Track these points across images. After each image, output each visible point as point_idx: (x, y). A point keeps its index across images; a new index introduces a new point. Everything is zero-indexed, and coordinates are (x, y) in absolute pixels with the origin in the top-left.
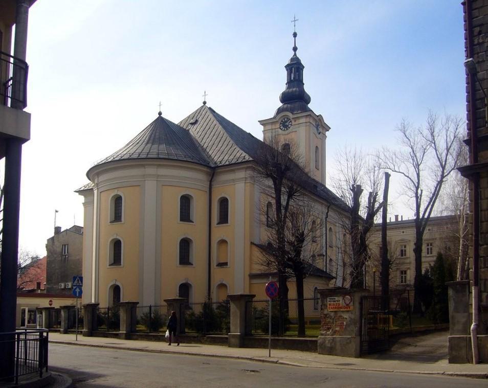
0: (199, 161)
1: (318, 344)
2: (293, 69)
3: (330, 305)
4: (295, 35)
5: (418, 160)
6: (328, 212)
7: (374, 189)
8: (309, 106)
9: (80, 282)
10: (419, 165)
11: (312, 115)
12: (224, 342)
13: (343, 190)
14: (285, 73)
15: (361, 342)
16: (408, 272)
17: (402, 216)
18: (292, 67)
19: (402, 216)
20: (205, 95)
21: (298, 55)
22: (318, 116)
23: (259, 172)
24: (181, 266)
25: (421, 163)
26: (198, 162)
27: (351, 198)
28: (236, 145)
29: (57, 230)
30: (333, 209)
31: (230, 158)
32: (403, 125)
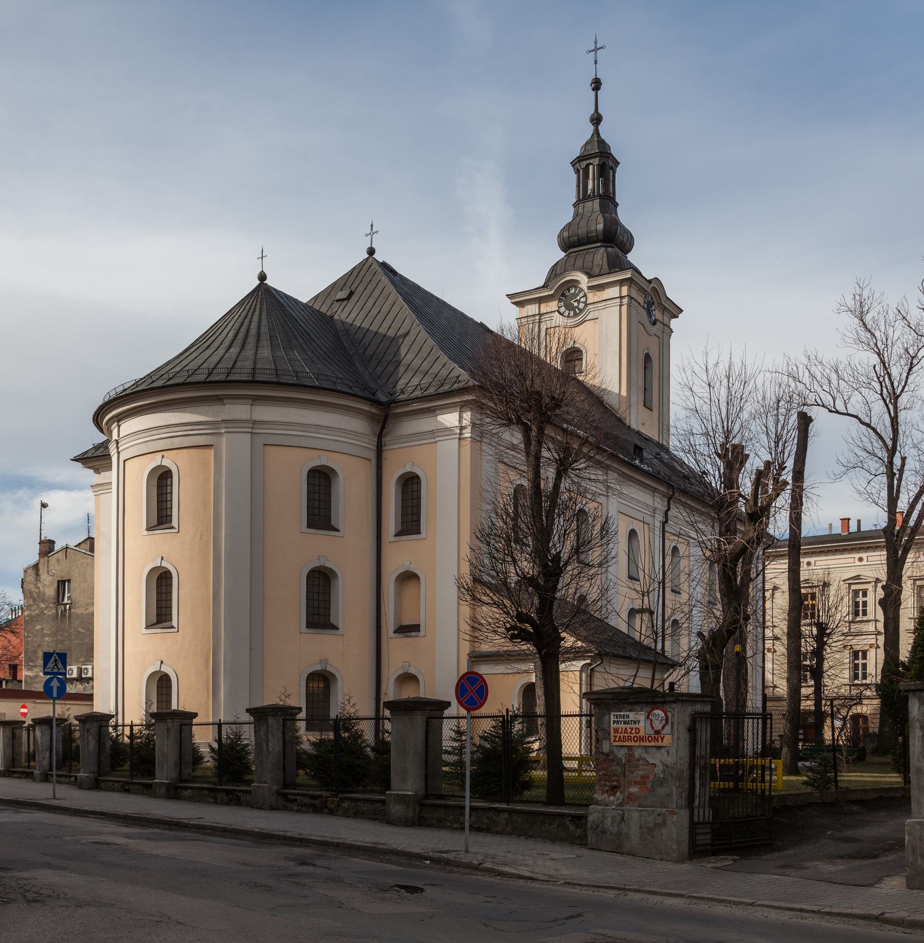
0: (351, 387)
1: (589, 826)
2: (591, 167)
3: (616, 730)
4: (597, 85)
5: (896, 384)
6: (669, 509)
7: (776, 454)
8: (632, 257)
9: (60, 666)
10: (897, 398)
11: (637, 278)
12: (381, 815)
13: (699, 457)
14: (572, 178)
15: (693, 825)
16: (871, 654)
17: (859, 521)
18: (588, 165)
19: (859, 521)
20: (372, 233)
21: (603, 136)
22: (650, 282)
23: (496, 415)
24: (312, 631)
25: (902, 391)
26: (349, 391)
27: (717, 477)
28: (441, 348)
29: (47, 547)
30: (684, 505)
31: (422, 382)
32: (857, 298)
